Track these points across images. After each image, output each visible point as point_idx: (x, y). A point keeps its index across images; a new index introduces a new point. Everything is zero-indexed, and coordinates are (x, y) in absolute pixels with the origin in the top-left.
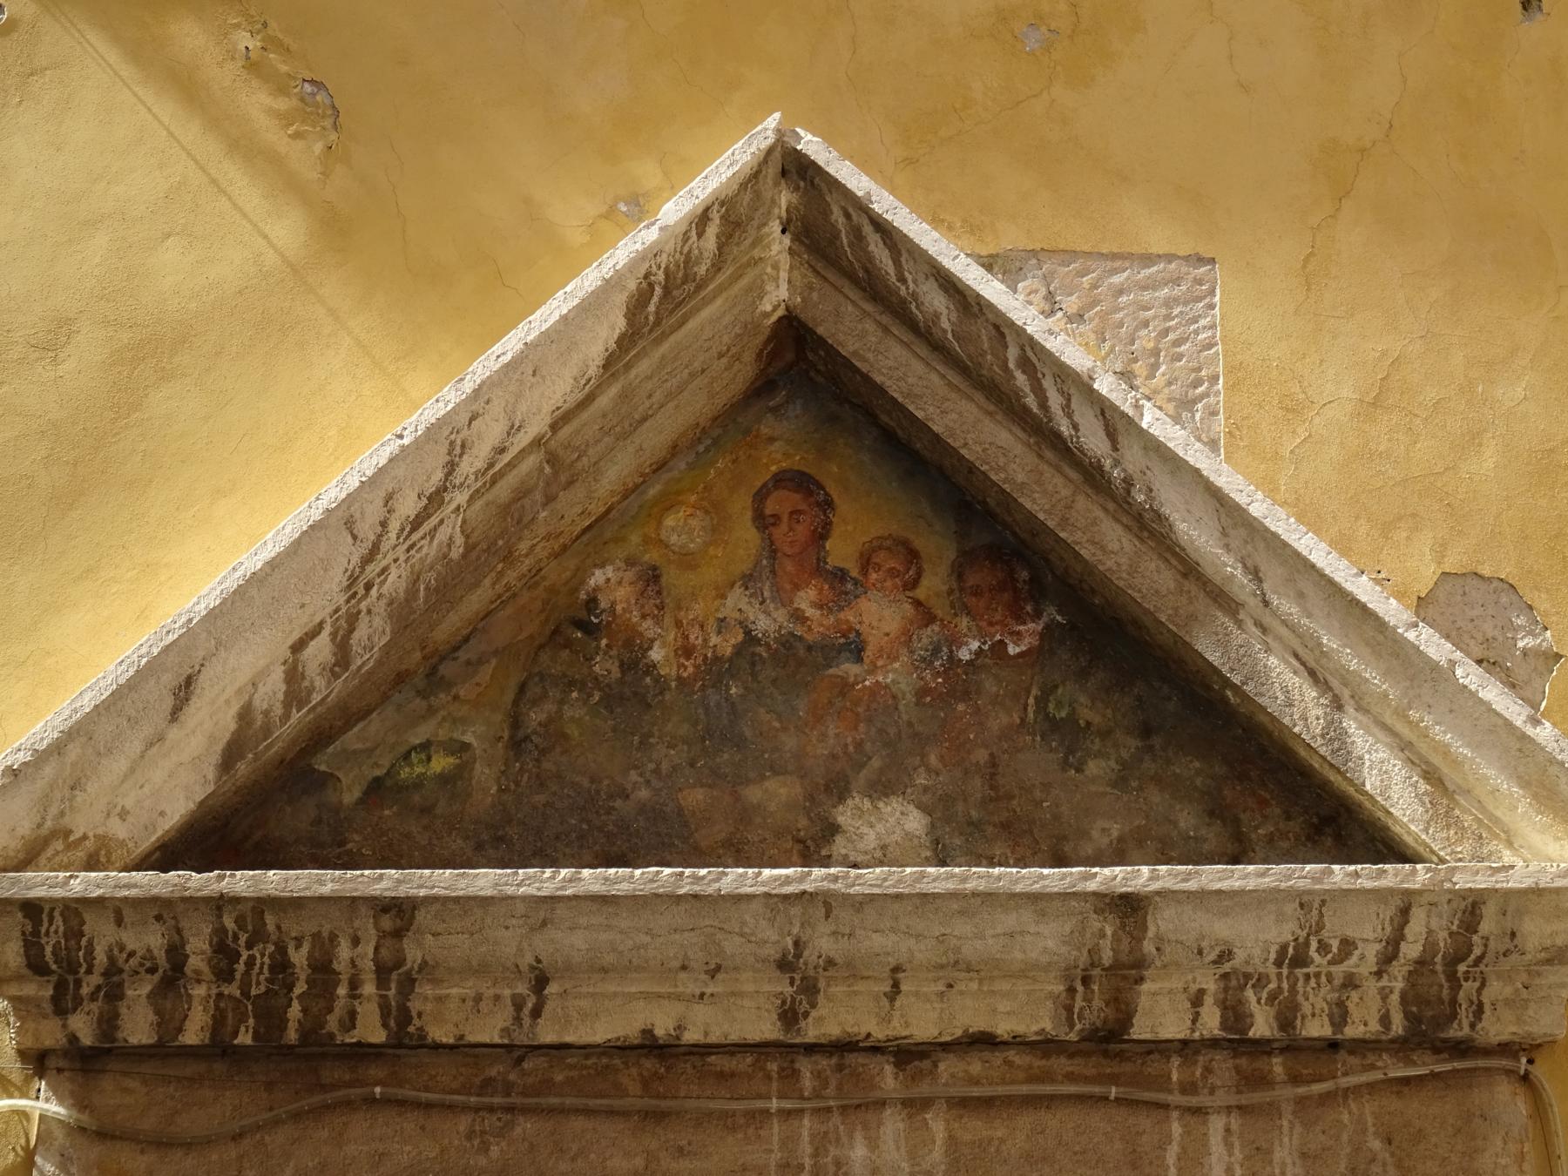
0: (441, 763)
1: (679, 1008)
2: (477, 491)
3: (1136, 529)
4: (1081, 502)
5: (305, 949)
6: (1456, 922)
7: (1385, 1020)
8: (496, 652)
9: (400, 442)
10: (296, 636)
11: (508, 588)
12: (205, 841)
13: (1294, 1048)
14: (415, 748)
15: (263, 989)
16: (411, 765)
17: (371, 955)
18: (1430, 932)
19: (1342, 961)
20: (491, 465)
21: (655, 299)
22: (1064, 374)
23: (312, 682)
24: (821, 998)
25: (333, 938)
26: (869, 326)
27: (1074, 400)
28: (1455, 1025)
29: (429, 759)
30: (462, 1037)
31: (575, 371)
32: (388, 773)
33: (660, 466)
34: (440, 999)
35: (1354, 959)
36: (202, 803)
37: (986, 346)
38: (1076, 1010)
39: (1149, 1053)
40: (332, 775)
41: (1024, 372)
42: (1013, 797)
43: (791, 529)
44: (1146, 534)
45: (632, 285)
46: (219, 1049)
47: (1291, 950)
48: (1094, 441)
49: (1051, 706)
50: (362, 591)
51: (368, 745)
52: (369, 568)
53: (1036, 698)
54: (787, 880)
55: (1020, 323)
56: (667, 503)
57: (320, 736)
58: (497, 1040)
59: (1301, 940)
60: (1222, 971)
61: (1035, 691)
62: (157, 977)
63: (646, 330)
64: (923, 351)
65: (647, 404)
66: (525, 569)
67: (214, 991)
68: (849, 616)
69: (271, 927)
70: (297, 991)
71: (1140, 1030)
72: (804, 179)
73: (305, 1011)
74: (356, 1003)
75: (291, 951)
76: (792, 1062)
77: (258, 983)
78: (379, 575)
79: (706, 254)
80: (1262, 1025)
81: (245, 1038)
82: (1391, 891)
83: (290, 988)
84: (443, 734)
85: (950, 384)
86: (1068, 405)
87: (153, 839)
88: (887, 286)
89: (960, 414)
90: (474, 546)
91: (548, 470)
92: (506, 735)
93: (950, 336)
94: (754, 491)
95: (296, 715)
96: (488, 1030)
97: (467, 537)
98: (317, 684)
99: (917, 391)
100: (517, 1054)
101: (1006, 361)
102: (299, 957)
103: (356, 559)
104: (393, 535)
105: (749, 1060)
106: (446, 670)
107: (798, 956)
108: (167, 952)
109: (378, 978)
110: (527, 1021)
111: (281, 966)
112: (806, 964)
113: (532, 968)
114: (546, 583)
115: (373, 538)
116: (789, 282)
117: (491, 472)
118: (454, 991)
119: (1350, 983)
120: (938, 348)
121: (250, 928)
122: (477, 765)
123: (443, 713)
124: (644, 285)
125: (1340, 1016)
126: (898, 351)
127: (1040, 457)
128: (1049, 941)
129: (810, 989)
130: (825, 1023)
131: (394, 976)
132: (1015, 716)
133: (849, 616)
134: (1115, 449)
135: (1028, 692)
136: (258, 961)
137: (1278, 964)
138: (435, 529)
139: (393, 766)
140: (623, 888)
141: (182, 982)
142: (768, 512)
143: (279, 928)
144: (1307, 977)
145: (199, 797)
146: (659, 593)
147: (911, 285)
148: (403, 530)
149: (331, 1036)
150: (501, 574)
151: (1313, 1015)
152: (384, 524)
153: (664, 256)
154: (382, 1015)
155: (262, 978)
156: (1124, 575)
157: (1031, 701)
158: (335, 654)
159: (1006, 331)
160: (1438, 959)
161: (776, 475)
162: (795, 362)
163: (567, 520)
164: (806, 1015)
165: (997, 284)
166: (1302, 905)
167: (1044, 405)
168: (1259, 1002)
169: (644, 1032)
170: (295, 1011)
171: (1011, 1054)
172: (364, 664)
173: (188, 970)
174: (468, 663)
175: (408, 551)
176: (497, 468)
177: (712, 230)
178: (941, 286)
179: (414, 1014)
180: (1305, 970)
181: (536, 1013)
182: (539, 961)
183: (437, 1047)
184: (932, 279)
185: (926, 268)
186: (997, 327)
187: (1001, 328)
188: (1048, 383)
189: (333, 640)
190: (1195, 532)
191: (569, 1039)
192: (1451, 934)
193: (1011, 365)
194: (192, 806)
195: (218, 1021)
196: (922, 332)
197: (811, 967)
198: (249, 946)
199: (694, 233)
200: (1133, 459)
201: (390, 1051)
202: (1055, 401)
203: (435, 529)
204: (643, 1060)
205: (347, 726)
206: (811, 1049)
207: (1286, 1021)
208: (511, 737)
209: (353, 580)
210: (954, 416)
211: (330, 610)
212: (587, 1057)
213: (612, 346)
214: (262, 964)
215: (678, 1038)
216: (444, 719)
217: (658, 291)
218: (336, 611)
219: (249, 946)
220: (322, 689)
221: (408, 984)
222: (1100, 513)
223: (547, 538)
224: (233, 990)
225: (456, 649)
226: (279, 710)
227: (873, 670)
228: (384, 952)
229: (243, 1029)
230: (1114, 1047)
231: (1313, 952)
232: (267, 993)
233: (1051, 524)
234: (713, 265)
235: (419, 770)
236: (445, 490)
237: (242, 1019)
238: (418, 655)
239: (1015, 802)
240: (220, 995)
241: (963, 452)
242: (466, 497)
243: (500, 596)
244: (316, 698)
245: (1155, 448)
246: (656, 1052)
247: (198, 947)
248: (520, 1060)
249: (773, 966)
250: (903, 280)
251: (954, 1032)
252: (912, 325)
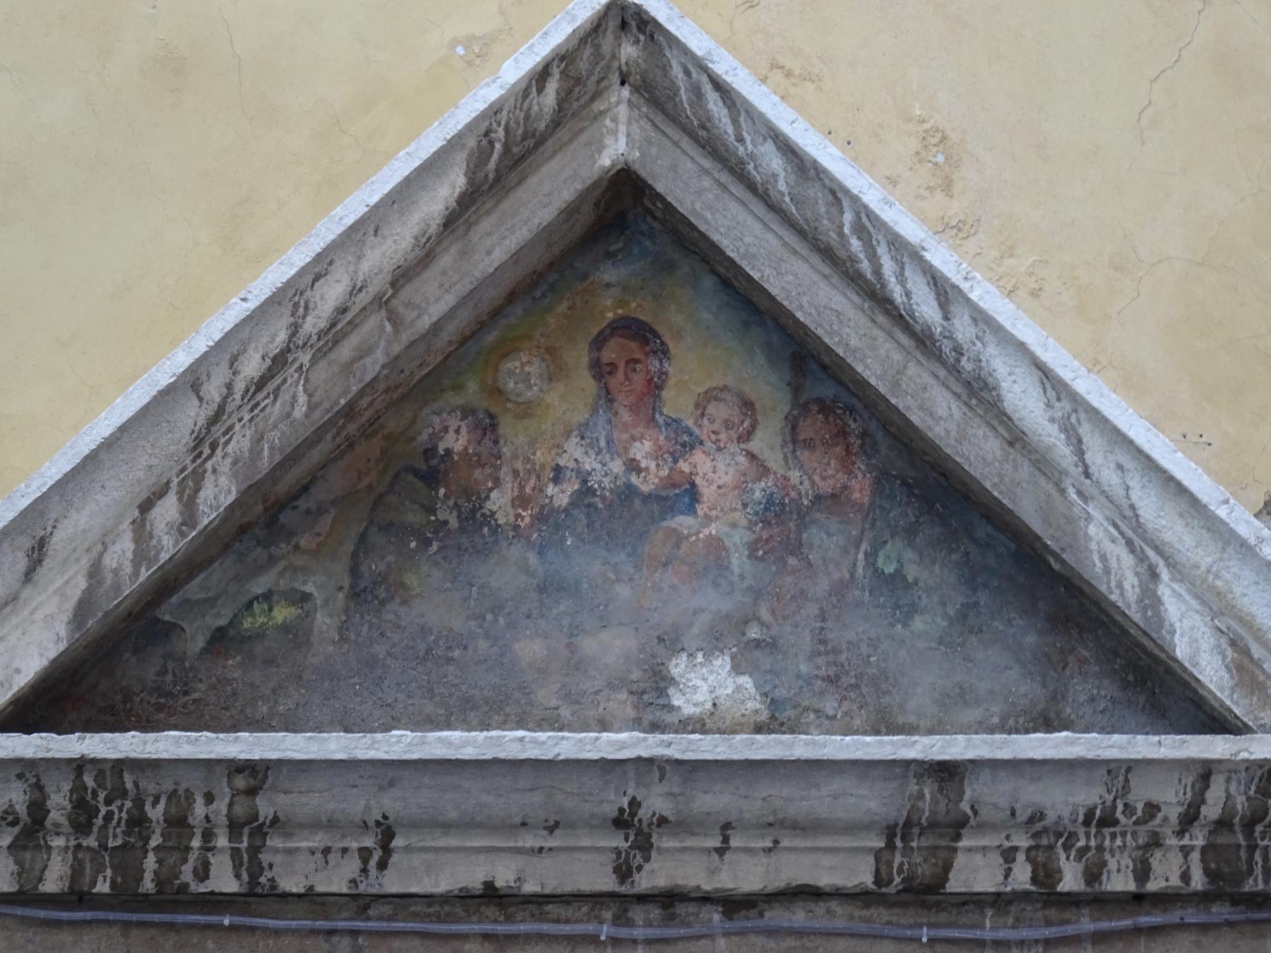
0: (282, 613)
1: (521, 861)
2: (319, 350)
3: (965, 396)
4: (912, 369)
5: (161, 807)
6: (1253, 788)
7: (1186, 877)
8: (334, 502)
9: (245, 305)
10: (144, 495)
11: (347, 438)
13: (1101, 902)
14: (257, 598)
15: (119, 842)
16: (253, 615)
17: (225, 812)
18: (1229, 797)
19: (1146, 822)
20: (333, 325)
21: (495, 157)
22: (897, 243)
23: (159, 541)
24: (654, 854)
25: (189, 795)
26: (707, 182)
27: (907, 267)
28: (1251, 881)
29: (271, 610)
30: (311, 888)
31: (416, 230)
32: (231, 623)
33: (496, 314)
34: (290, 852)
35: (1158, 820)
36: (54, 661)
37: (823, 210)
38: (896, 866)
39: (964, 904)
40: (175, 625)
41: (859, 238)
42: (841, 652)
43: (627, 379)
44: (974, 402)
45: (472, 143)
46: (77, 897)
47: (1098, 812)
48: (927, 309)
49: (880, 561)
50: (207, 451)
51: (211, 594)
52: (214, 429)
53: (866, 553)
54: (623, 746)
55: (855, 191)
56: (505, 350)
57: (165, 586)
58: (345, 890)
59: (1109, 803)
60: (1034, 831)
61: (864, 546)
62: (16, 830)
63: (486, 187)
64: (759, 208)
65: (487, 261)
66: (364, 419)
67: (73, 843)
68: (684, 466)
69: (129, 785)
70: (153, 843)
71: (955, 884)
72: (644, 33)
73: (160, 862)
74: (209, 855)
75: (148, 808)
76: (626, 911)
77: (115, 836)
78: (224, 434)
79: (546, 110)
80: (1071, 879)
81: (103, 887)
82: (1194, 761)
83: (146, 840)
84: (284, 584)
85: (786, 245)
86: (902, 274)
87: (9, 695)
88: (725, 145)
89: (796, 276)
90: (318, 405)
91: (389, 328)
92: (346, 585)
93: (787, 199)
94: (590, 339)
95: (144, 574)
96: (336, 880)
97: (310, 396)
98: (165, 542)
99: (753, 250)
100: (361, 902)
101: (841, 227)
102: (156, 813)
103: (201, 421)
104: (238, 396)
105: (585, 909)
106: (286, 518)
107: (633, 814)
108: (28, 807)
109: (231, 833)
110: (373, 871)
111: (138, 822)
112: (640, 820)
113: (378, 824)
114: (386, 432)
115: (218, 399)
116: (628, 135)
117: (334, 331)
118: (304, 844)
119: (1155, 842)
120: (774, 208)
121: (109, 785)
122: (319, 616)
123: (283, 563)
124: (485, 142)
125: (1143, 872)
126: (734, 207)
127: (874, 321)
128: (874, 802)
129: (644, 846)
130: (655, 875)
131: (246, 831)
132: (845, 571)
133: (684, 466)
134: (946, 318)
135: (858, 547)
136: (116, 817)
137: (1087, 823)
138: (278, 388)
139: (235, 616)
140: (468, 753)
141: (41, 834)
142: (605, 360)
143: (136, 785)
144: (1113, 836)
145: (52, 654)
146: (496, 442)
147: (750, 147)
148: (247, 390)
149: (187, 885)
150: (343, 427)
151: (1119, 871)
152: (229, 386)
153: (505, 113)
154: (234, 867)
155: (118, 830)
156: (953, 442)
157: (861, 556)
158: (181, 513)
159: (840, 195)
160: (1236, 820)
161: (612, 322)
163: (407, 373)
164: (640, 868)
165: (834, 150)
166: (1109, 772)
167: (878, 272)
168: (1068, 858)
169: (485, 883)
170: (150, 862)
171: (834, 904)
172: (210, 523)
173: (48, 823)
174: (308, 512)
175: (252, 410)
176: (339, 327)
177: (552, 87)
178: (778, 148)
179: (265, 865)
180: (1112, 830)
181: (382, 865)
182: (385, 817)
183: (286, 896)
184: (770, 142)
185: (764, 131)
186: (833, 192)
187: (837, 193)
188: (882, 250)
189: (180, 500)
190: (1023, 399)
191: (413, 890)
192: (1248, 799)
193: (846, 230)
194: (45, 663)
195: (77, 871)
196: (759, 192)
197: (645, 824)
198: (108, 802)
199: (534, 90)
200: (963, 329)
201: (242, 899)
202: (888, 267)
203: (278, 388)
204: (483, 909)
205: (190, 577)
206: (642, 898)
207: (1092, 875)
208: (352, 587)
209: (199, 441)
210: (790, 277)
211: (176, 470)
212: (429, 906)
213: (452, 203)
214: (120, 819)
215: (519, 888)
216: (285, 569)
217: (498, 146)
218: (182, 471)
219: (108, 802)
220: (168, 546)
221: (260, 833)
222: (928, 379)
223: (386, 391)
224: (91, 841)
225: (295, 497)
226: (128, 569)
227: (708, 519)
228: (238, 809)
229: (100, 878)
230: (931, 898)
231: (1119, 815)
232: (124, 845)
233: (882, 390)
234: (552, 121)
235: (261, 620)
236: (289, 350)
237: (100, 869)
238: (261, 507)
239: (843, 657)
240: (79, 847)
241: (799, 315)
242: (309, 357)
243: (339, 446)
244: (164, 557)
245: (981, 318)
246: (496, 900)
247: (59, 802)
248: (365, 908)
249: (610, 824)
250: (741, 140)
251: (778, 883)
252: (751, 187)
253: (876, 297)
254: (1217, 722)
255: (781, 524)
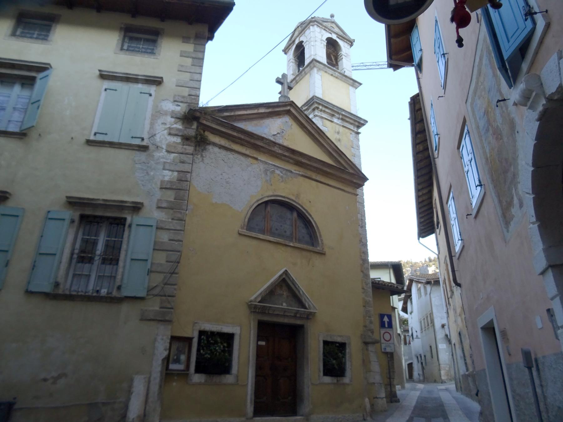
12: (259, 302)
162: (284, 280)
190: (301, 292)
253: (295, 286)
254: (306, 308)
255: (287, 297)
